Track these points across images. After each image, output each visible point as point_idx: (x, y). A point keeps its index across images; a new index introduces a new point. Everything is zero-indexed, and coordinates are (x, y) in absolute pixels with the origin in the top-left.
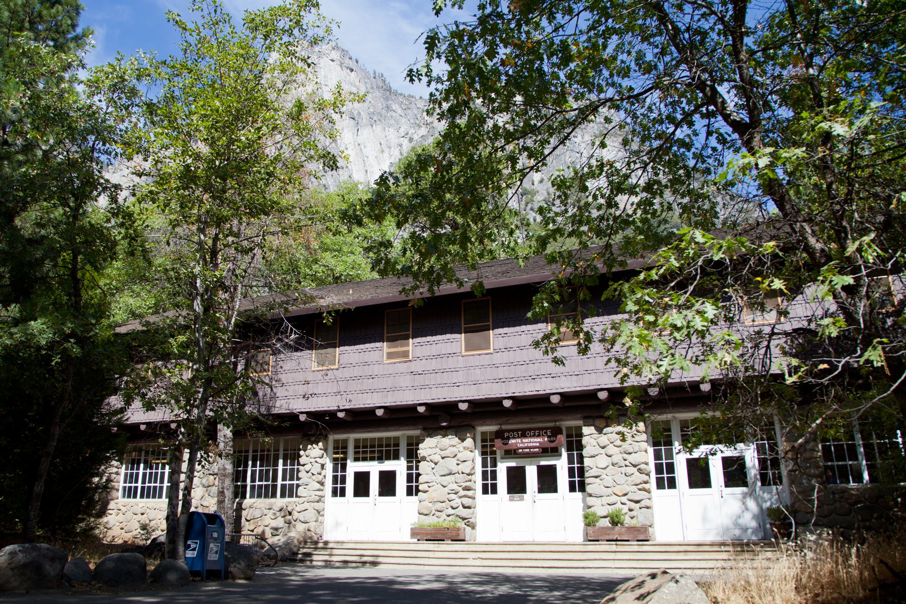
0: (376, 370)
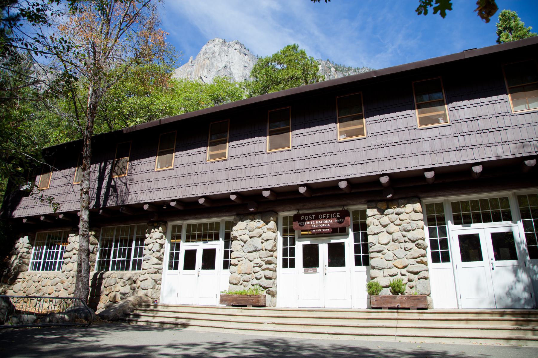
0: (201, 168)
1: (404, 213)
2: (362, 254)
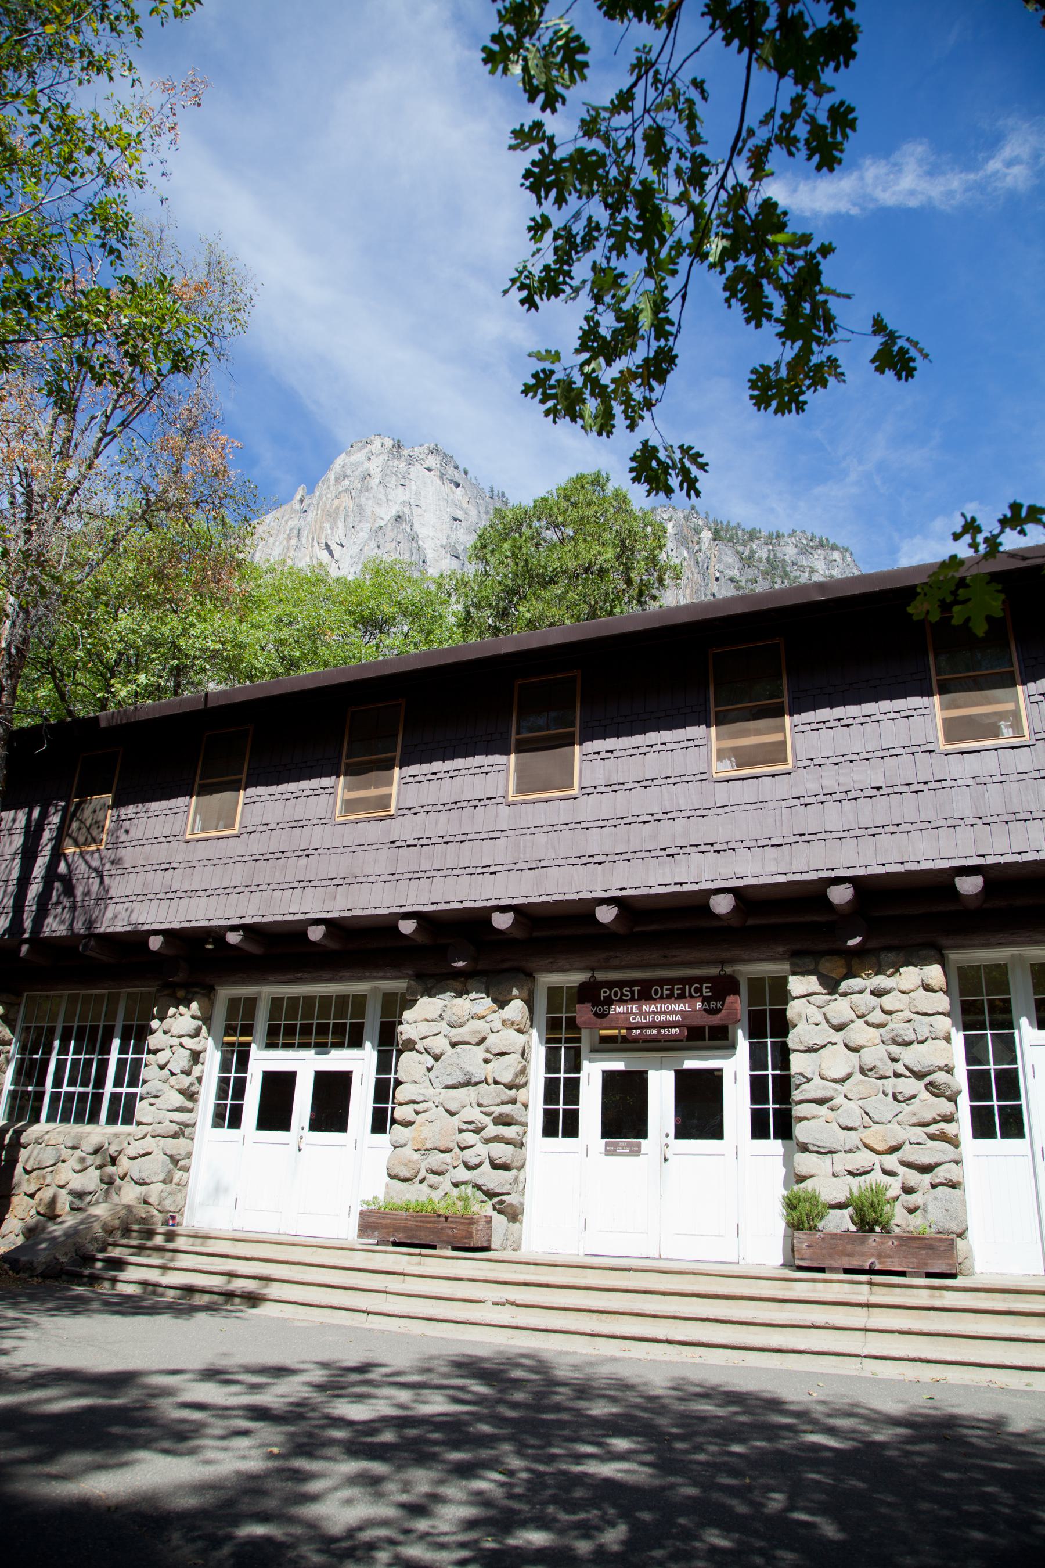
0: (318, 837)
1: (896, 993)
2: (771, 1106)
